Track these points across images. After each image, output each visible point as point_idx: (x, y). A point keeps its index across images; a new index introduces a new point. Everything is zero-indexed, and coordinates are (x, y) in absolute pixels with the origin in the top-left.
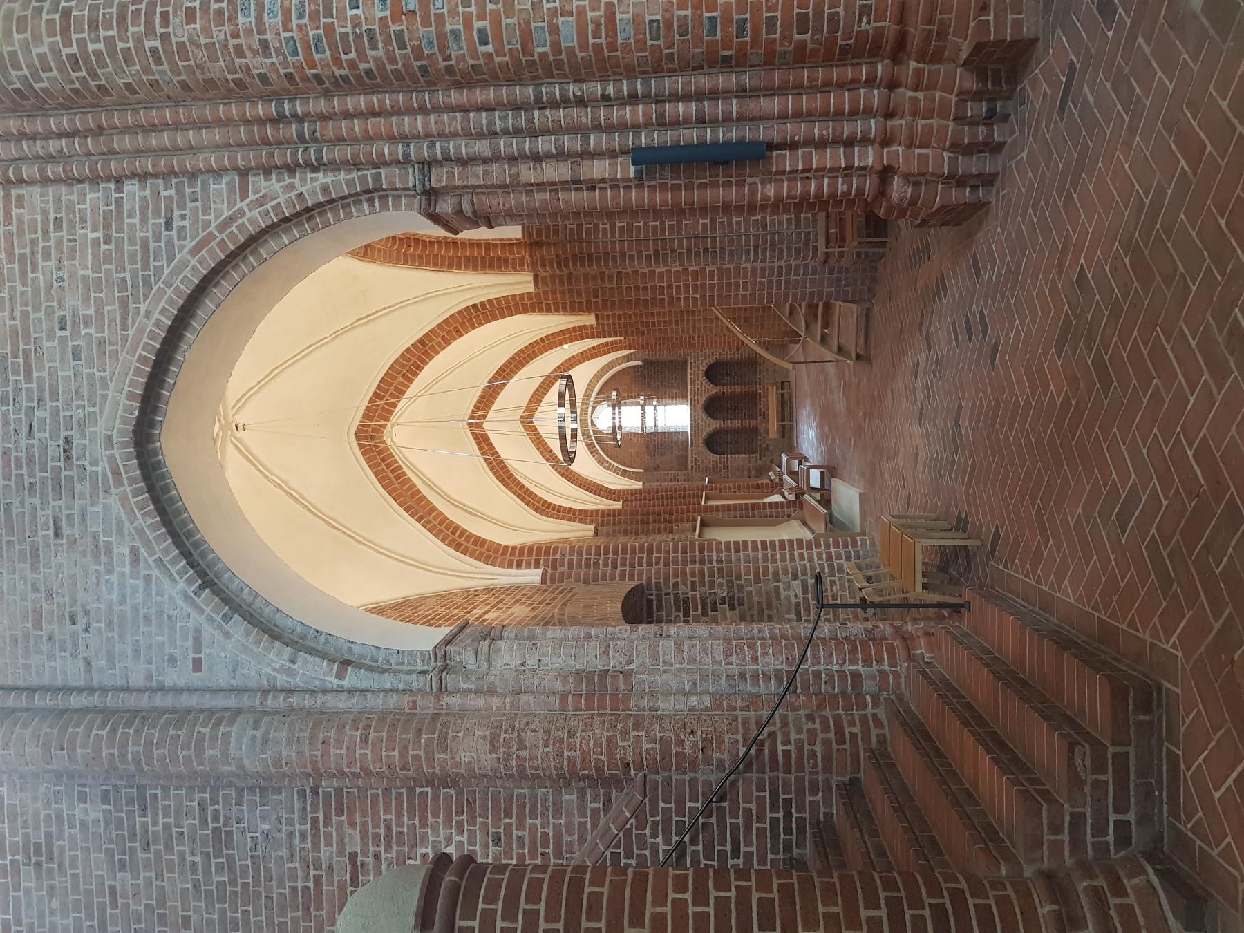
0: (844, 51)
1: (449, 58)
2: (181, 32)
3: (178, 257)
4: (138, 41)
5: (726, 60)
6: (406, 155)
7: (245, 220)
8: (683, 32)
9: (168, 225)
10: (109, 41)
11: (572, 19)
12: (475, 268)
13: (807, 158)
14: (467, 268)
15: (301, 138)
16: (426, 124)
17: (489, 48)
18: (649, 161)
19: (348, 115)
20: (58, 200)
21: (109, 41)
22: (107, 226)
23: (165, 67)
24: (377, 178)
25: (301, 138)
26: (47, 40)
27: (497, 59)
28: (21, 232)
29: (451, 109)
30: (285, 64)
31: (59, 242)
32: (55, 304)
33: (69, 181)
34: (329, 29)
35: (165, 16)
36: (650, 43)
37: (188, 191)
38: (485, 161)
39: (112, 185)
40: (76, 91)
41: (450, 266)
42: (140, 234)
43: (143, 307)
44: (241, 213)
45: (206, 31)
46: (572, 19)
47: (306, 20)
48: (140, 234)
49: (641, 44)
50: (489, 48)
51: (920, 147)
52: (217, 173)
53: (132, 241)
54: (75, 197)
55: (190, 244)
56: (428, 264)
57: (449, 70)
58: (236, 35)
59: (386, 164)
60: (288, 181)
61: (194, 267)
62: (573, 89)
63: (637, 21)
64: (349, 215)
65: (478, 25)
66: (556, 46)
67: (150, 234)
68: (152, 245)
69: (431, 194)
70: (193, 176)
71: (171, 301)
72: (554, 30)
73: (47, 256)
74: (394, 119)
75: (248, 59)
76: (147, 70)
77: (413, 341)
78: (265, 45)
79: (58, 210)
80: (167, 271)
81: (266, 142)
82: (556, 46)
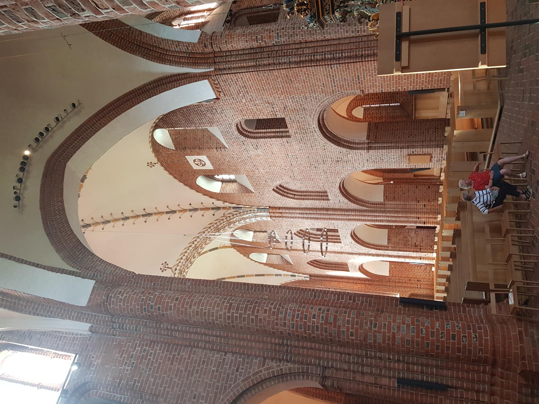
0: (474, 361)
1: (340, 338)
2: (261, 315)
3: (238, 382)
4: (249, 315)
5: (432, 356)
6: (319, 364)
7: (262, 374)
8: (418, 345)
9: (237, 371)
10: (241, 314)
11: (381, 334)
12: (322, 399)
13: (462, 394)
14: (319, 398)
15: (287, 351)
16: (328, 355)
17: (353, 338)
18: (402, 382)
19: (303, 348)
20: (206, 355)
21: (241, 314)
22: (218, 367)
23: (254, 324)
24: (308, 369)
25: (287, 351)
26: (224, 311)
27: (355, 341)
28: (192, 362)
29: (337, 352)
30: (289, 330)
31: (202, 368)
32: (194, 389)
33: (212, 350)
34: (305, 323)
35: (258, 310)
36: (406, 346)
37: (246, 360)
38: (345, 370)
39: (223, 354)
40: (226, 325)
41: (313, 396)
42: (227, 372)
43: (222, 397)
44: (261, 371)
45: (269, 316)
46: (381, 334)
47: (298, 319)
48: (227, 372)
49: (403, 346)
50: (353, 338)
51: (506, 399)
52: (256, 357)
53: (224, 373)
54: (211, 355)
55: (242, 378)
56: (305, 394)
57: (339, 341)
58: (277, 319)
59: (311, 365)
60: (279, 364)
61: (242, 387)
62: (378, 354)
63: (402, 339)
64: (295, 379)
65: (351, 330)
66: (375, 341)
67: (231, 372)
68: (230, 376)
69: (324, 378)
70: (249, 356)
71: (231, 397)
72: (375, 336)
73: (197, 372)
74: (317, 352)
75: (279, 327)
76: (248, 324)
77: (83, 323)
78: (285, 324)
79: (205, 358)
80: (233, 386)
81: (275, 350)
82: (375, 341)
